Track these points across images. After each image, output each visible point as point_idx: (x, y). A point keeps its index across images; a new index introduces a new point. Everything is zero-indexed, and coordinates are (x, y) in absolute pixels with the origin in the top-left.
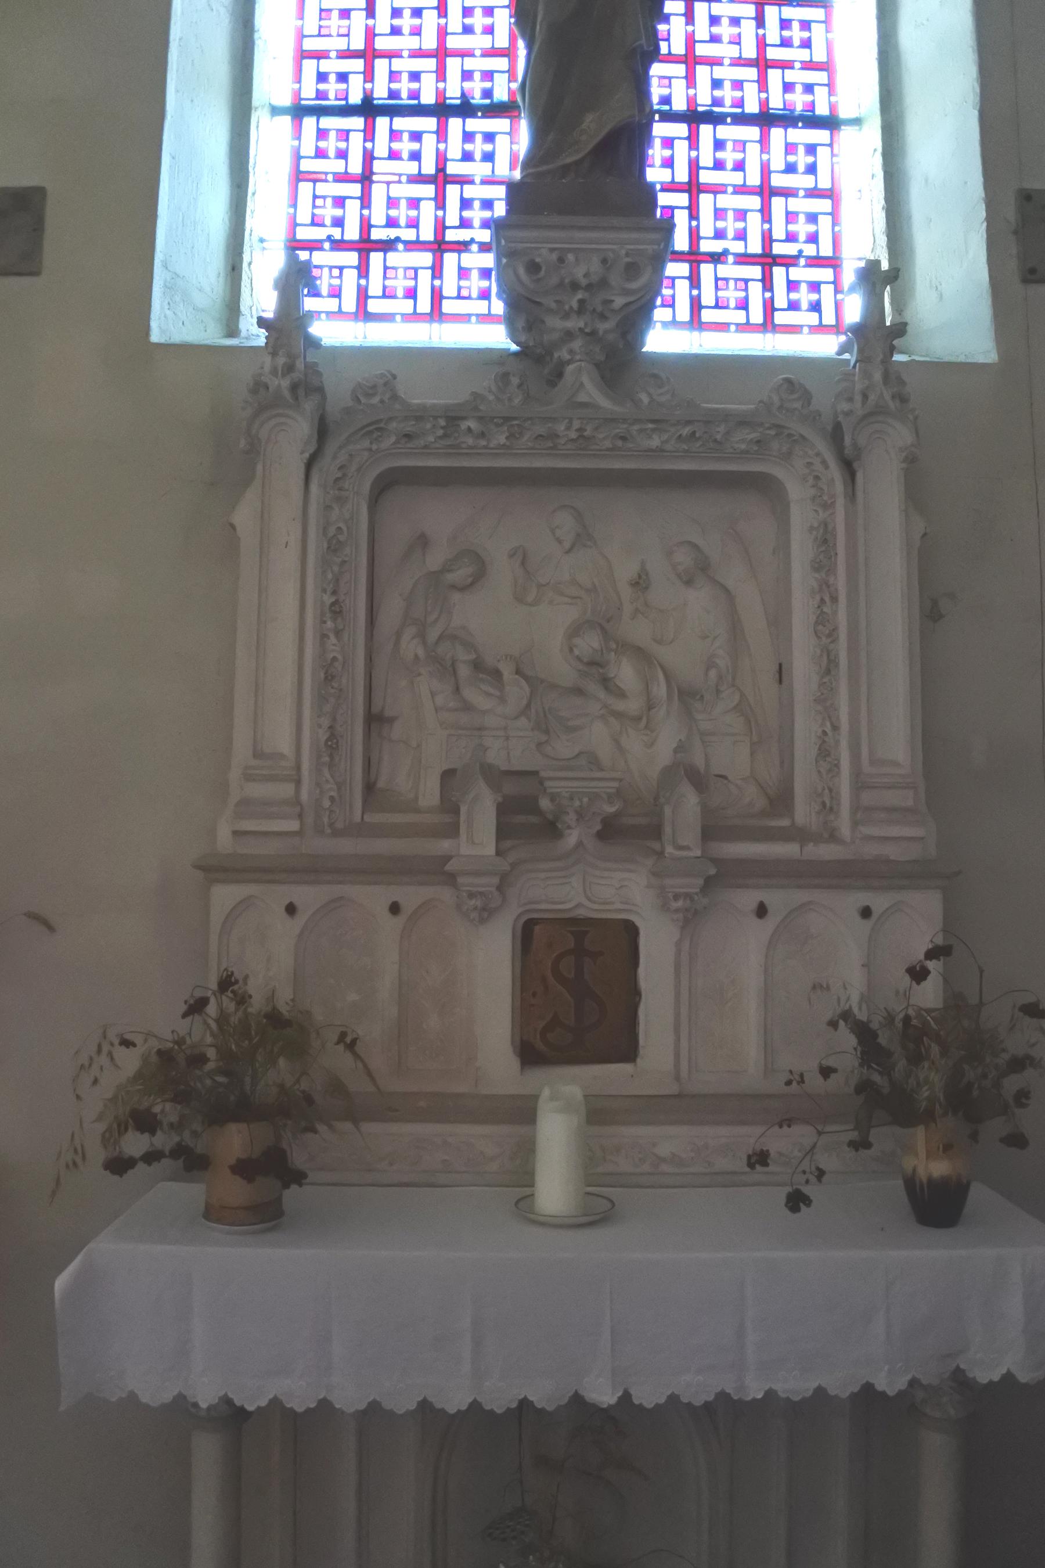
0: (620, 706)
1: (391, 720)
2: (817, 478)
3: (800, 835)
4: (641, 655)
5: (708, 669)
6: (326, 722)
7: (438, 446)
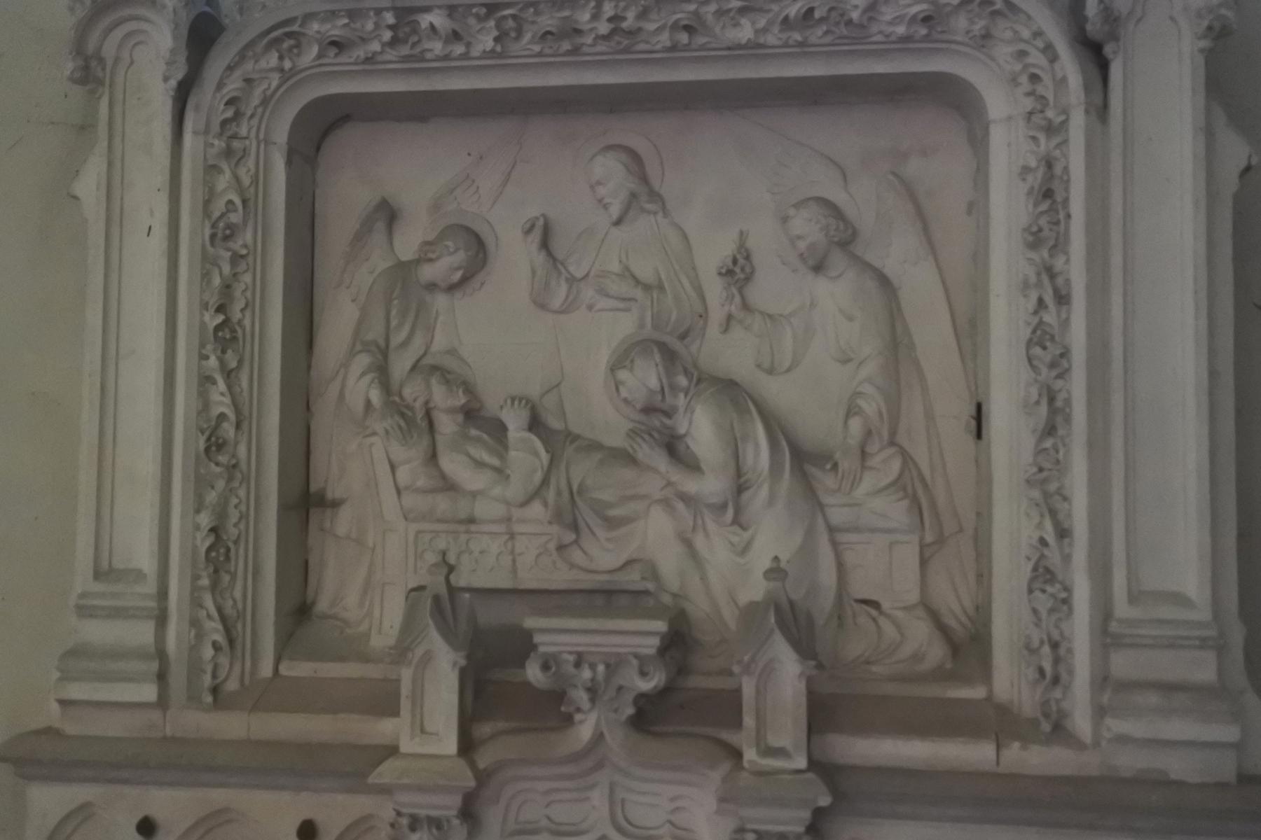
0: (691, 485)
1: (336, 504)
2: (1034, 78)
3: (1000, 723)
4: (731, 392)
5: (848, 415)
6: (205, 520)
7: (387, 57)
